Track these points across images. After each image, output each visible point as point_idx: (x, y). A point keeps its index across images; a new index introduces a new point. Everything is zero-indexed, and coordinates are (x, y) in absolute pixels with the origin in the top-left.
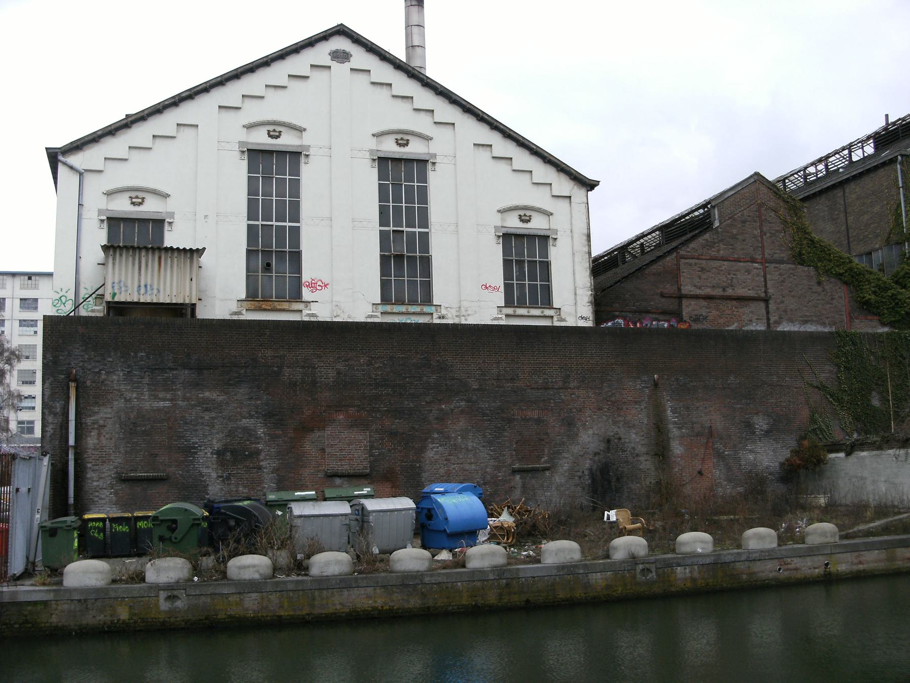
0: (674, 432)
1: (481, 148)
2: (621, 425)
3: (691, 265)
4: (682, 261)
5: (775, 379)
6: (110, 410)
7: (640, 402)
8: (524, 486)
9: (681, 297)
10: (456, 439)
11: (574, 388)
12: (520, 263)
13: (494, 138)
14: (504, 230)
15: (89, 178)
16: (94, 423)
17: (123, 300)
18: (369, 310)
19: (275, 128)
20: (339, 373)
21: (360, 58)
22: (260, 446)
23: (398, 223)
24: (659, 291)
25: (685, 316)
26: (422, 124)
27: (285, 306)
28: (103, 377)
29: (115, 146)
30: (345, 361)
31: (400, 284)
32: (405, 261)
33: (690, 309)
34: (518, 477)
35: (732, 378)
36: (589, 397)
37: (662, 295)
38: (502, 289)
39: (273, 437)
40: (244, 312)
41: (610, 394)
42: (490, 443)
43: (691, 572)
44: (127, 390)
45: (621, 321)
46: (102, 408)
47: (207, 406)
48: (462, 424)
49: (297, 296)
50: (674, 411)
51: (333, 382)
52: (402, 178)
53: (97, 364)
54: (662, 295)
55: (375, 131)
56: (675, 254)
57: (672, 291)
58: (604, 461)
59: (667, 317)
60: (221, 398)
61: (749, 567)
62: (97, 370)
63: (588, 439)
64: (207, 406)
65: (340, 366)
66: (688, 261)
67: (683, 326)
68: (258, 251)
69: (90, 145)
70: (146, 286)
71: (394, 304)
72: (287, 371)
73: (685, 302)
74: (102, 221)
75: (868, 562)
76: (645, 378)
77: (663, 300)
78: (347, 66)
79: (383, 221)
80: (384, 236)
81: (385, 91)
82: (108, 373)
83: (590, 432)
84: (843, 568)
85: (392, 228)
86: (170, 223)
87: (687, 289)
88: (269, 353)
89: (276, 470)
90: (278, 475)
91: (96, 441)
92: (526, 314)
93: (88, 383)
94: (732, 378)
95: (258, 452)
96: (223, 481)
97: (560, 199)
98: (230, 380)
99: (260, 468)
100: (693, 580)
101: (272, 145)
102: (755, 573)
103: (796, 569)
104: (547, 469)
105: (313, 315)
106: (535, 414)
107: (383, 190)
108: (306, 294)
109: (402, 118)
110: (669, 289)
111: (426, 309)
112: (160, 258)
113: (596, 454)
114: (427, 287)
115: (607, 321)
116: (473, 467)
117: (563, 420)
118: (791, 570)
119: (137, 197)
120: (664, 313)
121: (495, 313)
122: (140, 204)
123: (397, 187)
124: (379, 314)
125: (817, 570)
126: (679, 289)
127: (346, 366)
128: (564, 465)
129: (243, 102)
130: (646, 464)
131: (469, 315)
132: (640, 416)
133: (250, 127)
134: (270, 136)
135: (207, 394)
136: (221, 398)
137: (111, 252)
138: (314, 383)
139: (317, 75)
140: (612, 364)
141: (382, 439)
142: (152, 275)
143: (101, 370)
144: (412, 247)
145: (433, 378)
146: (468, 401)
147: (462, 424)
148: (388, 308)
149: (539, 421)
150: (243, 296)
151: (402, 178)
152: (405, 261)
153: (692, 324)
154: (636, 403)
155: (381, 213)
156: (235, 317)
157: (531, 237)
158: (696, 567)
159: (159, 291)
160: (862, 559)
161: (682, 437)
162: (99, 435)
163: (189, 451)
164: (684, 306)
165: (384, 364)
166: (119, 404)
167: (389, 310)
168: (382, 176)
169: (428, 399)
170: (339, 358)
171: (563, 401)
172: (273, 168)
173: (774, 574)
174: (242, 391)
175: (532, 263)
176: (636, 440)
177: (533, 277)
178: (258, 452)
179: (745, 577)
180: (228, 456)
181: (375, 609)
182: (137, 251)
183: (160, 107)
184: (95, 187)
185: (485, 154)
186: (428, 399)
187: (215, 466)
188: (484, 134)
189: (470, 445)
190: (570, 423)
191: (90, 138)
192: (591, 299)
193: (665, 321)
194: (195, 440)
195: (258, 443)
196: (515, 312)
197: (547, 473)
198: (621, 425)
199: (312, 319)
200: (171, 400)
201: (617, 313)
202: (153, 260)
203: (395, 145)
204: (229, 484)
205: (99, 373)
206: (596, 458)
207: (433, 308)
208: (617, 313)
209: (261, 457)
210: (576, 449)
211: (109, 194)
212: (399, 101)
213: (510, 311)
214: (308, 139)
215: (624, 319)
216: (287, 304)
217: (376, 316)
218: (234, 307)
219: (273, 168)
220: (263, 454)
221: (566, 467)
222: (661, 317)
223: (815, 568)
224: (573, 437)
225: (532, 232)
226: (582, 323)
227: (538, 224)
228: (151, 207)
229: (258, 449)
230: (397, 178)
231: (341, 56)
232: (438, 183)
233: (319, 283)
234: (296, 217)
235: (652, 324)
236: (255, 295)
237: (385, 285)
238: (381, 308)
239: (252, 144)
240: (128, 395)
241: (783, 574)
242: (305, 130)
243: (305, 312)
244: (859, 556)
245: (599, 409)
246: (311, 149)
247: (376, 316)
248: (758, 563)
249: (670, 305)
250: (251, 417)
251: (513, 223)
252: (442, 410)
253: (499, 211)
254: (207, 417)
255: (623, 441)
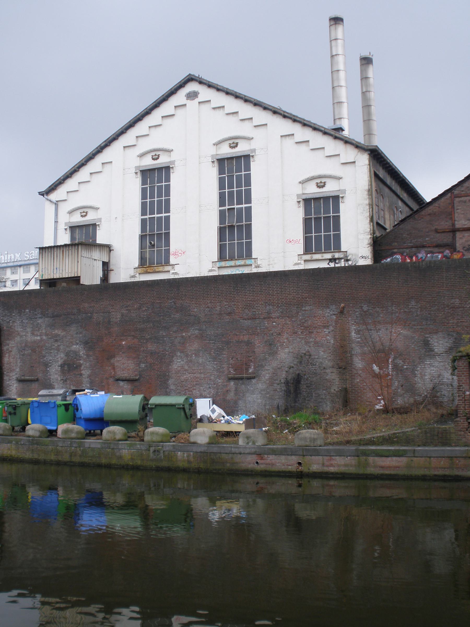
0: (357, 350)
1: (287, 137)
2: (311, 345)
3: (465, 202)
4: (457, 199)
5: (457, 301)
6: (13, 342)
7: (328, 326)
8: (236, 390)
9: (454, 231)
10: (191, 356)
11: (275, 318)
12: (318, 220)
13: (296, 129)
14: (304, 197)
15: (61, 205)
16: (7, 350)
17: (46, 278)
18: (210, 266)
19: (155, 153)
20: (122, 315)
21: (205, 93)
22: (81, 362)
23: (231, 203)
24: (433, 228)
25: (459, 245)
26: (245, 130)
27: (161, 269)
28: (11, 324)
29: (71, 184)
30: (126, 307)
31: (232, 246)
32: (235, 231)
33: (463, 240)
34: (232, 383)
35: (413, 303)
36: (286, 324)
37: (437, 231)
38: (302, 241)
39: (88, 356)
40: (137, 275)
41: (304, 321)
42: (215, 359)
43: (188, 456)
44: (21, 331)
45: (398, 257)
46: (10, 341)
47: (56, 338)
48: (196, 345)
49: (167, 262)
50: (358, 332)
51: (119, 321)
52: (234, 170)
53: (8, 317)
54: (437, 231)
55: (214, 142)
56: (449, 194)
57: (446, 227)
58: (297, 372)
59: (441, 250)
60: (63, 334)
61: (232, 458)
62: (8, 321)
63: (285, 356)
64: (56, 338)
65: (124, 311)
66: (462, 199)
67: (456, 256)
68: (147, 235)
69: (60, 186)
70: (57, 269)
71: (236, 260)
72: (95, 315)
73: (458, 235)
74: (66, 229)
75: (339, 466)
76: (334, 307)
77: (438, 235)
78: (197, 101)
79: (222, 203)
80: (222, 214)
81: (220, 112)
82: (14, 322)
83: (287, 350)
84: (315, 468)
85: (227, 207)
86: (342, 197)
87: (458, 226)
88: (86, 305)
89: (89, 376)
90: (90, 379)
91: (8, 360)
92: (321, 258)
93: (5, 328)
94: (413, 303)
95: (80, 365)
96: (63, 382)
97: (348, 165)
98: (67, 322)
99: (81, 375)
100: (189, 462)
101: (155, 164)
102: (237, 463)
103: (273, 464)
104: (254, 378)
105: (176, 273)
106: (246, 338)
107: (144, 191)
108: (173, 260)
109: (233, 128)
110: (445, 224)
111: (248, 262)
112: (63, 251)
113: (290, 367)
114: (338, 238)
115: (386, 258)
116: (203, 376)
117: (266, 342)
118: (267, 464)
119: (84, 212)
120: (438, 246)
121: (296, 260)
122: (85, 216)
123: (152, 188)
124: (216, 269)
125: (290, 467)
126: (453, 225)
127: (127, 310)
128: (266, 375)
129: (137, 141)
130: (333, 376)
131: (275, 264)
132: (328, 337)
133: (142, 156)
134: (153, 159)
135: (56, 331)
136: (63, 334)
137: (73, 247)
138: (109, 322)
139: (180, 112)
140: (306, 298)
141: (146, 357)
142: (60, 261)
143: (10, 321)
144: (239, 219)
145: (177, 316)
146: (200, 330)
147: (196, 345)
148: (223, 264)
149: (248, 343)
150: (137, 264)
151: (234, 170)
152: (235, 231)
153: (465, 253)
154: (324, 327)
155: (220, 198)
156: (133, 280)
157: (326, 199)
158: (192, 453)
159: (63, 270)
160: (333, 462)
161: (364, 354)
162: (9, 356)
163: (46, 365)
164: (457, 239)
165: (148, 308)
166: (18, 339)
167: (224, 265)
168: (221, 171)
169: (175, 329)
170: (123, 305)
171: (267, 328)
172: (155, 180)
173: (252, 465)
174: (73, 329)
175: (327, 219)
176: (324, 357)
177: (327, 229)
178: (80, 365)
179: (228, 465)
180: (66, 367)
181: (11, 456)
182: (53, 249)
183: (91, 155)
184: (64, 208)
185: (289, 142)
186: (175, 329)
187: (59, 374)
188: (287, 127)
189: (200, 360)
190: (270, 344)
191: (58, 182)
192: (370, 241)
193: (439, 253)
194: (51, 358)
195: (80, 360)
196: (312, 257)
197: (254, 381)
198: (311, 345)
199: (176, 277)
200: (40, 335)
201: (395, 250)
202: (60, 253)
203: (229, 147)
204: (66, 384)
205: (9, 322)
206: (291, 370)
207: (253, 261)
208: (395, 250)
209: (82, 368)
210: (275, 364)
211: (71, 212)
212: (231, 116)
213: (308, 257)
214: (174, 156)
215: (402, 254)
216: (162, 267)
217: (214, 270)
218: (132, 272)
219: (155, 180)
220: (83, 367)
221: (267, 376)
222: (436, 250)
223: (290, 465)
224: (274, 354)
225: (328, 195)
226: (362, 262)
227: (331, 188)
228: (91, 217)
229: (80, 363)
230: (230, 171)
231: (192, 96)
232: (257, 170)
233: (180, 252)
234: (249, 200)
235: (426, 256)
236: (145, 263)
237: (222, 249)
238: (218, 264)
239: (143, 166)
240: (22, 334)
241: (262, 467)
242: (172, 150)
243: (172, 271)
244: (330, 460)
245: (294, 333)
246: (176, 163)
247: (214, 270)
248: (239, 456)
249: (446, 238)
250: (77, 344)
251: (312, 190)
252: (183, 337)
253: (300, 182)
254: (56, 345)
255: (313, 357)
